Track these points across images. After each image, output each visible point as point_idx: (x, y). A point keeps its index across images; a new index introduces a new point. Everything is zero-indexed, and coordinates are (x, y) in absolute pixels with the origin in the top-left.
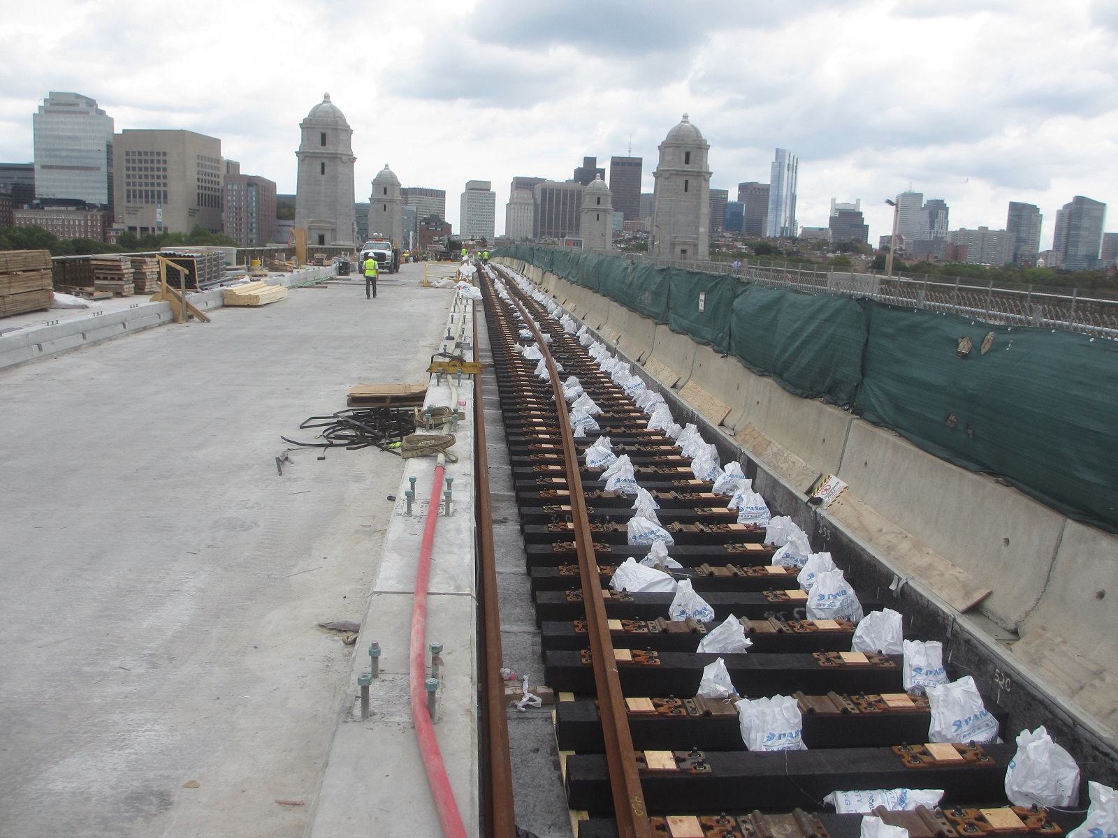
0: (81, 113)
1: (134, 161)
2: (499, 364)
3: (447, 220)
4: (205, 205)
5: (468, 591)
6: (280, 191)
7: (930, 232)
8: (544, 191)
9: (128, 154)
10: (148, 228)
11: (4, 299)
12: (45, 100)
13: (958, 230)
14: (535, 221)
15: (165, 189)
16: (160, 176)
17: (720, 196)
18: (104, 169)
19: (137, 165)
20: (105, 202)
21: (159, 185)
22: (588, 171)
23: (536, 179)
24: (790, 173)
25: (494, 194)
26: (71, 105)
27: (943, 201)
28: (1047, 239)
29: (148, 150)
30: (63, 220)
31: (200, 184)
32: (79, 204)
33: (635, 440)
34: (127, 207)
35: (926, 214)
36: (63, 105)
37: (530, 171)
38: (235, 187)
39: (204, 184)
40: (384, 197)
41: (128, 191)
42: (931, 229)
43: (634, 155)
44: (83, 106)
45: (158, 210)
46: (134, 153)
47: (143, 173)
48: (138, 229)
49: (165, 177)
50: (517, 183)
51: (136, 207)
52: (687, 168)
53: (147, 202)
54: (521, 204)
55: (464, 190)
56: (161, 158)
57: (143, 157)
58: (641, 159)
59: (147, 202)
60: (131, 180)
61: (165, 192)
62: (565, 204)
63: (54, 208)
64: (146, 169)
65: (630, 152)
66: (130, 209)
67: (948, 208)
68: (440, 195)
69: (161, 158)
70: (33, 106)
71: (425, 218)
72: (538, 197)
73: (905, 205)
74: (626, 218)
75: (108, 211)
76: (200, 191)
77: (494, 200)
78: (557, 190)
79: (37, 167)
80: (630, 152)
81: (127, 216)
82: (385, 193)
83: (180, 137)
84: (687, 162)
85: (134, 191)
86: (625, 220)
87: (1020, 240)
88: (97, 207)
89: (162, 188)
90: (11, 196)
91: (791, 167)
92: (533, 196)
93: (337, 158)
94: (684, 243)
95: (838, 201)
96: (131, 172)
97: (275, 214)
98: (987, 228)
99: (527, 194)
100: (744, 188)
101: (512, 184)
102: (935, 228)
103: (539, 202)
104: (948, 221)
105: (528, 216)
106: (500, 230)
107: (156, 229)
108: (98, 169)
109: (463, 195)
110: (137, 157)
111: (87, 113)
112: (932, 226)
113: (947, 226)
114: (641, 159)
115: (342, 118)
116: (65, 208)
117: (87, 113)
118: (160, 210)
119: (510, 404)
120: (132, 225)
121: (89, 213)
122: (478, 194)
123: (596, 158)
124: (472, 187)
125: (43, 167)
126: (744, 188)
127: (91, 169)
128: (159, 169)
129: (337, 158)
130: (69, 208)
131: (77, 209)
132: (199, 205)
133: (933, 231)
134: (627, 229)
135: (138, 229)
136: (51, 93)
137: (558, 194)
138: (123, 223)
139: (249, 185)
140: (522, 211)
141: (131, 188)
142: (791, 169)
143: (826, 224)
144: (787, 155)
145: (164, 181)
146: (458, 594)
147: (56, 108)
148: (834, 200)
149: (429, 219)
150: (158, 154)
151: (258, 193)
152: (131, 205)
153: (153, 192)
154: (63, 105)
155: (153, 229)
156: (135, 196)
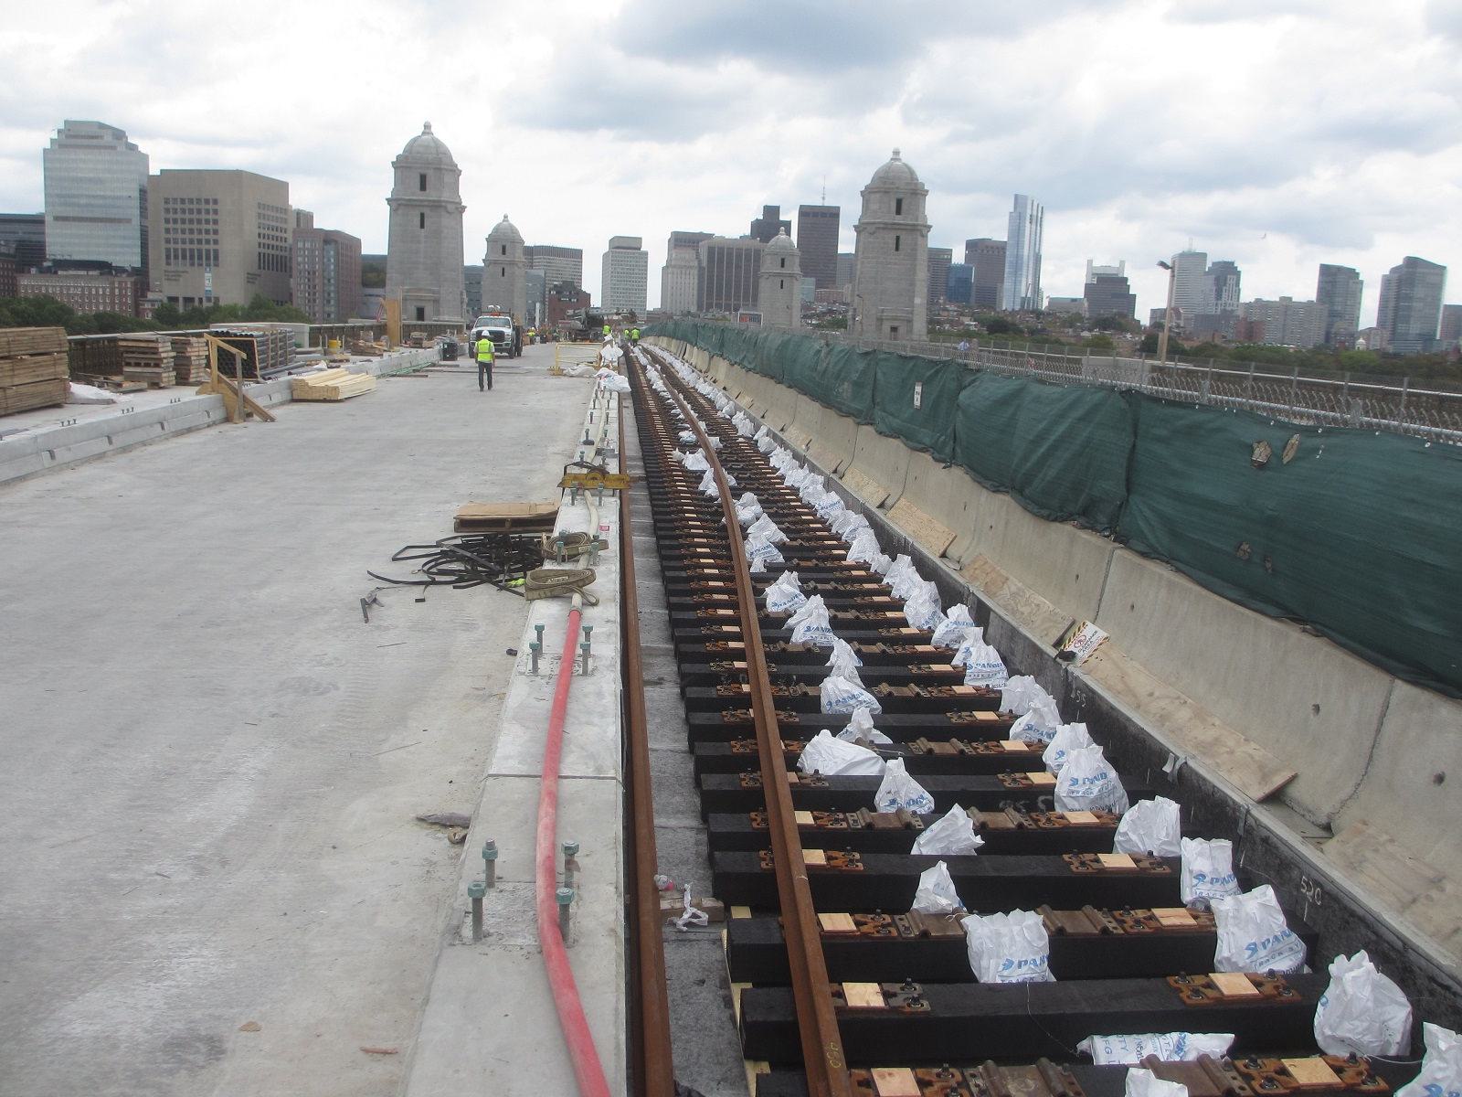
0: (105, 147)
1: (175, 211)
2: (653, 477)
3: (585, 287)
4: (268, 269)
5: (611, 774)
6: (366, 250)
7: (1217, 304)
8: (711, 250)
9: (167, 201)
10: (193, 299)
11: (5, 391)
12: (59, 131)
13: (1253, 300)
14: (700, 289)
15: (216, 247)
16: (209, 230)
17: (942, 257)
18: (136, 221)
19: (179, 216)
20: (138, 265)
21: (208, 242)
22: (769, 223)
23: (701, 234)
24: (1034, 227)
25: (646, 253)
26: (92, 137)
27: (1233, 263)
28: (1369, 313)
29: (194, 196)
30: (83, 288)
31: (262, 241)
32: (104, 267)
33: (830, 576)
34: (165, 271)
35: (1211, 280)
36: (83, 137)
37: (693, 224)
38: (308, 245)
39: (266, 241)
40: (502, 258)
41: (168, 250)
42: (1218, 299)
43: (829, 202)
44: (108, 139)
45: (206, 274)
46: (175, 200)
47: (187, 226)
48: (181, 300)
49: (216, 232)
50: (676, 240)
51: (177, 272)
52: (899, 219)
53: (192, 264)
54: (681, 267)
55: (606, 249)
56: (211, 207)
57: (187, 206)
58: (839, 208)
59: (192, 264)
60: (171, 236)
61: (216, 252)
62: (738, 267)
63: (71, 272)
64: (191, 221)
65: (824, 198)
66: (171, 274)
67: (1240, 272)
68: (576, 255)
69: (211, 207)
70: (43, 139)
71: (556, 286)
72: (704, 257)
73: (1183, 268)
74: (819, 285)
75: (141, 276)
76: (262, 250)
77: (646, 262)
78: (728, 248)
79: (49, 219)
80: (824, 198)
81: (165, 283)
82: (504, 252)
83: (236, 179)
84: (898, 212)
85: (176, 250)
86: (817, 288)
87: (1333, 315)
88: (127, 271)
89: (212, 247)
90: (14, 256)
91: (1034, 218)
92: (698, 257)
93: (440, 206)
94: (895, 319)
95: (1096, 264)
96: (171, 226)
97: (359, 280)
98: (1290, 298)
99: (689, 254)
100: (972, 246)
101: (669, 240)
102: (1223, 299)
103: (705, 264)
104: (1239, 290)
105: (691, 282)
106: (654, 301)
107: (204, 299)
108: (129, 221)
109: (605, 256)
110: (179, 206)
111: (113, 148)
112: (1219, 296)
113: (1239, 296)
114: (839, 208)
115: (447, 154)
116: (85, 273)
117: (113, 148)
118: (210, 275)
119: (667, 529)
120: (173, 295)
121: (117, 279)
122: (625, 253)
123: (779, 207)
124: (617, 245)
125: (57, 218)
126: (972, 246)
127: (119, 221)
128: (207, 222)
129: (440, 206)
130: (91, 273)
131: (101, 274)
132: (260, 268)
133: (1219, 302)
134: (819, 299)
135: (181, 300)
136: (66, 122)
137: (730, 254)
138: (160, 292)
139: (326, 242)
140: (683, 276)
141: (172, 246)
142: (1034, 221)
143: (1080, 294)
144: (1029, 202)
145: (215, 237)
146: (599, 778)
147: (73, 141)
148: (1090, 262)
149: (561, 287)
150: (207, 202)
151: (337, 253)
152: (172, 268)
153: (200, 251)
154: (83, 137)
155: (201, 300)
156: (176, 257)
